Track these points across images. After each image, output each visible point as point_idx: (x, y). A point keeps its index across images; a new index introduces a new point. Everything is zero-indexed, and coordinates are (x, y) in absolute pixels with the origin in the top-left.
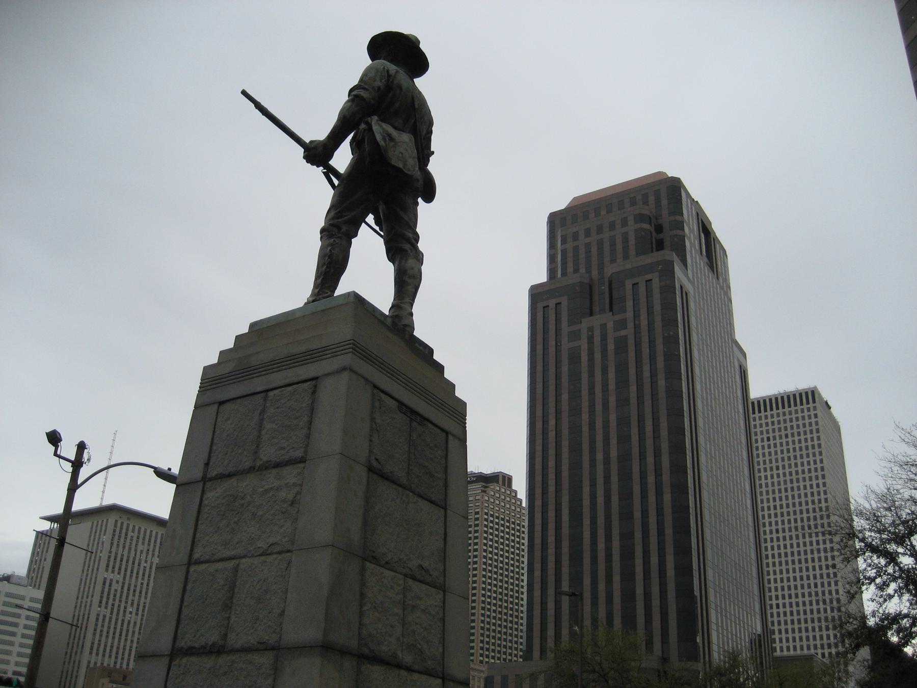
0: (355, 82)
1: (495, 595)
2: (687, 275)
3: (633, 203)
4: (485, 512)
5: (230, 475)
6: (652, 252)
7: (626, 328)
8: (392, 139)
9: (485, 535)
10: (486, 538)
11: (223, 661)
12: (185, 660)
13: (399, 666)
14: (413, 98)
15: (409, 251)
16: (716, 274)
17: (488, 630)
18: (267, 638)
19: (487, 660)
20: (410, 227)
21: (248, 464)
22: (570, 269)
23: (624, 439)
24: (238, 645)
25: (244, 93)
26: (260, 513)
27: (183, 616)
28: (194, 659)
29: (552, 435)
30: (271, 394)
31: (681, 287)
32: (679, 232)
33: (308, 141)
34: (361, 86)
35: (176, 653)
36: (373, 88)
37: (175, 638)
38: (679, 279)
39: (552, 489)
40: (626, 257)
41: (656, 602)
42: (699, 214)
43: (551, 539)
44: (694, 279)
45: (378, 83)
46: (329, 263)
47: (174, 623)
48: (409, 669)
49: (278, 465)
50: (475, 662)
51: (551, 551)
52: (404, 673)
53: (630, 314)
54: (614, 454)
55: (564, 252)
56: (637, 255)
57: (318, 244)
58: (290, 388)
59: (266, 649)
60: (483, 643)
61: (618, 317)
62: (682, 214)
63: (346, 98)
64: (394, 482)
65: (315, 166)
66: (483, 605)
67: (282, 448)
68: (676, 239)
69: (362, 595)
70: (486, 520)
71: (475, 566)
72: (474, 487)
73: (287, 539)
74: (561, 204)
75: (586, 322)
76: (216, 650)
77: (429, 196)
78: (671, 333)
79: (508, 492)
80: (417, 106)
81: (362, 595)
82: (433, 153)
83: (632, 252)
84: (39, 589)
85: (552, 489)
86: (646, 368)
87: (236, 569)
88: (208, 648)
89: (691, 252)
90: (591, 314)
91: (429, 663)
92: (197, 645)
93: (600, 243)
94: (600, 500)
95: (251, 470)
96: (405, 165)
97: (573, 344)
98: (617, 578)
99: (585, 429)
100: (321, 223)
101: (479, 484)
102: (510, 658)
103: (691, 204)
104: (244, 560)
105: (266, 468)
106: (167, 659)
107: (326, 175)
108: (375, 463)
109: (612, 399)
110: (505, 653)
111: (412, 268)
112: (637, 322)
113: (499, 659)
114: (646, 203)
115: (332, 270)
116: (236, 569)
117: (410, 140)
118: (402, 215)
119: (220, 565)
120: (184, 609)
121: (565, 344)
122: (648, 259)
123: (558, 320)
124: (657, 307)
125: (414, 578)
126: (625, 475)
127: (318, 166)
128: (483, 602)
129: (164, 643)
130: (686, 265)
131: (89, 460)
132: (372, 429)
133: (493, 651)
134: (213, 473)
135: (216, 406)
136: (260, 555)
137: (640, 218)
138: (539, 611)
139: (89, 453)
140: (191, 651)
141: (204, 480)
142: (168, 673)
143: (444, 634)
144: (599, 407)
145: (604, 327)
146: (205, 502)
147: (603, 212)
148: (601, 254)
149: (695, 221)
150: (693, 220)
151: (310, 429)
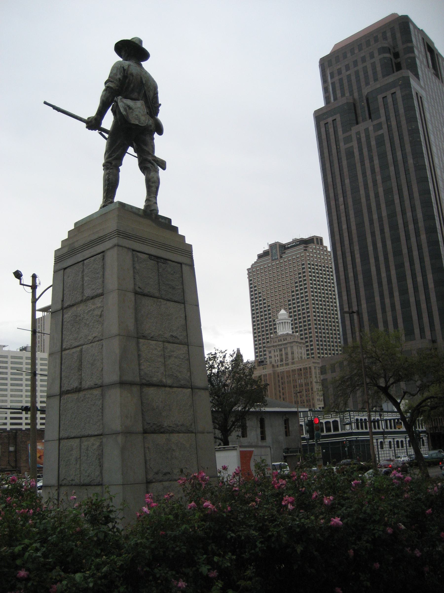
0: (107, 78)
1: (322, 315)
2: (419, 84)
3: (376, 40)
4: (309, 263)
5: (73, 305)
6: (394, 72)
7: (382, 128)
8: (130, 108)
9: (310, 278)
10: (311, 280)
11: (81, 394)
12: (66, 396)
13: (165, 386)
14: (141, 78)
15: (151, 168)
16: (440, 79)
17: (321, 337)
18: (97, 382)
19: (323, 356)
20: (150, 154)
21: (80, 299)
22: (339, 95)
23: (390, 203)
24: (86, 387)
25: (45, 103)
26: (88, 323)
27: (63, 375)
28: (69, 395)
29: (342, 207)
30: (85, 262)
31: (417, 94)
32: (411, 55)
33: (86, 119)
34: (109, 80)
35: (62, 393)
36: (116, 80)
37: (61, 387)
38: (415, 89)
39: (347, 242)
40: (376, 80)
41: (424, 306)
42: (425, 39)
43: (351, 275)
44: (425, 86)
45: (119, 76)
46: (108, 184)
47: (59, 380)
48: (171, 387)
49: (93, 298)
50: (315, 358)
51: (352, 284)
52: (168, 389)
53: (383, 119)
54: (384, 214)
55: (333, 84)
56: (384, 76)
57: (102, 172)
58: (93, 258)
59: (98, 387)
60: (319, 346)
61: (375, 122)
62: (411, 41)
63: (103, 87)
64: (151, 297)
65: (94, 131)
66: (316, 322)
67: (93, 289)
68: (409, 61)
69: (139, 356)
70: (310, 268)
71: (307, 298)
72: (291, 251)
73: (100, 334)
74: (327, 51)
75: (355, 129)
76: (78, 390)
77: (160, 131)
78: (414, 127)
79: (321, 248)
80: (144, 82)
81: (139, 356)
82: (160, 105)
83: (380, 75)
84: (44, 352)
85: (347, 242)
86: (399, 154)
87: (81, 351)
88: (75, 390)
89: (421, 68)
90: (357, 123)
91: (182, 382)
92: (69, 389)
93: (357, 73)
94: (379, 245)
95: (82, 301)
96: (140, 122)
97: (348, 145)
98: (396, 294)
99: (363, 200)
100: (103, 161)
101: (301, 246)
102: (337, 352)
103: (418, 33)
104: (84, 347)
105: (88, 300)
106: (58, 397)
107: (101, 134)
108: (139, 290)
109: (379, 178)
110: (333, 350)
111: (153, 177)
112: (389, 123)
113: (330, 354)
114: (385, 38)
115: (111, 188)
116: (81, 351)
117: (142, 105)
118: (145, 148)
119: (74, 350)
120: (62, 373)
121: (343, 146)
122: (391, 79)
123: (335, 132)
124: (402, 111)
125: (169, 342)
126: (394, 227)
127: (95, 130)
128: (315, 320)
129: (56, 390)
130: (418, 77)
131: (39, 284)
132: (134, 272)
133: (326, 349)
134: (66, 305)
135: (63, 271)
136: (91, 343)
137: (382, 50)
138: (349, 322)
139: (39, 280)
140: (68, 392)
141: (62, 309)
142: (60, 403)
143: (190, 367)
144: (370, 184)
145: (367, 130)
146: (64, 320)
147: (356, 51)
148: (358, 81)
149: (422, 44)
150: (420, 45)
151: (104, 278)
